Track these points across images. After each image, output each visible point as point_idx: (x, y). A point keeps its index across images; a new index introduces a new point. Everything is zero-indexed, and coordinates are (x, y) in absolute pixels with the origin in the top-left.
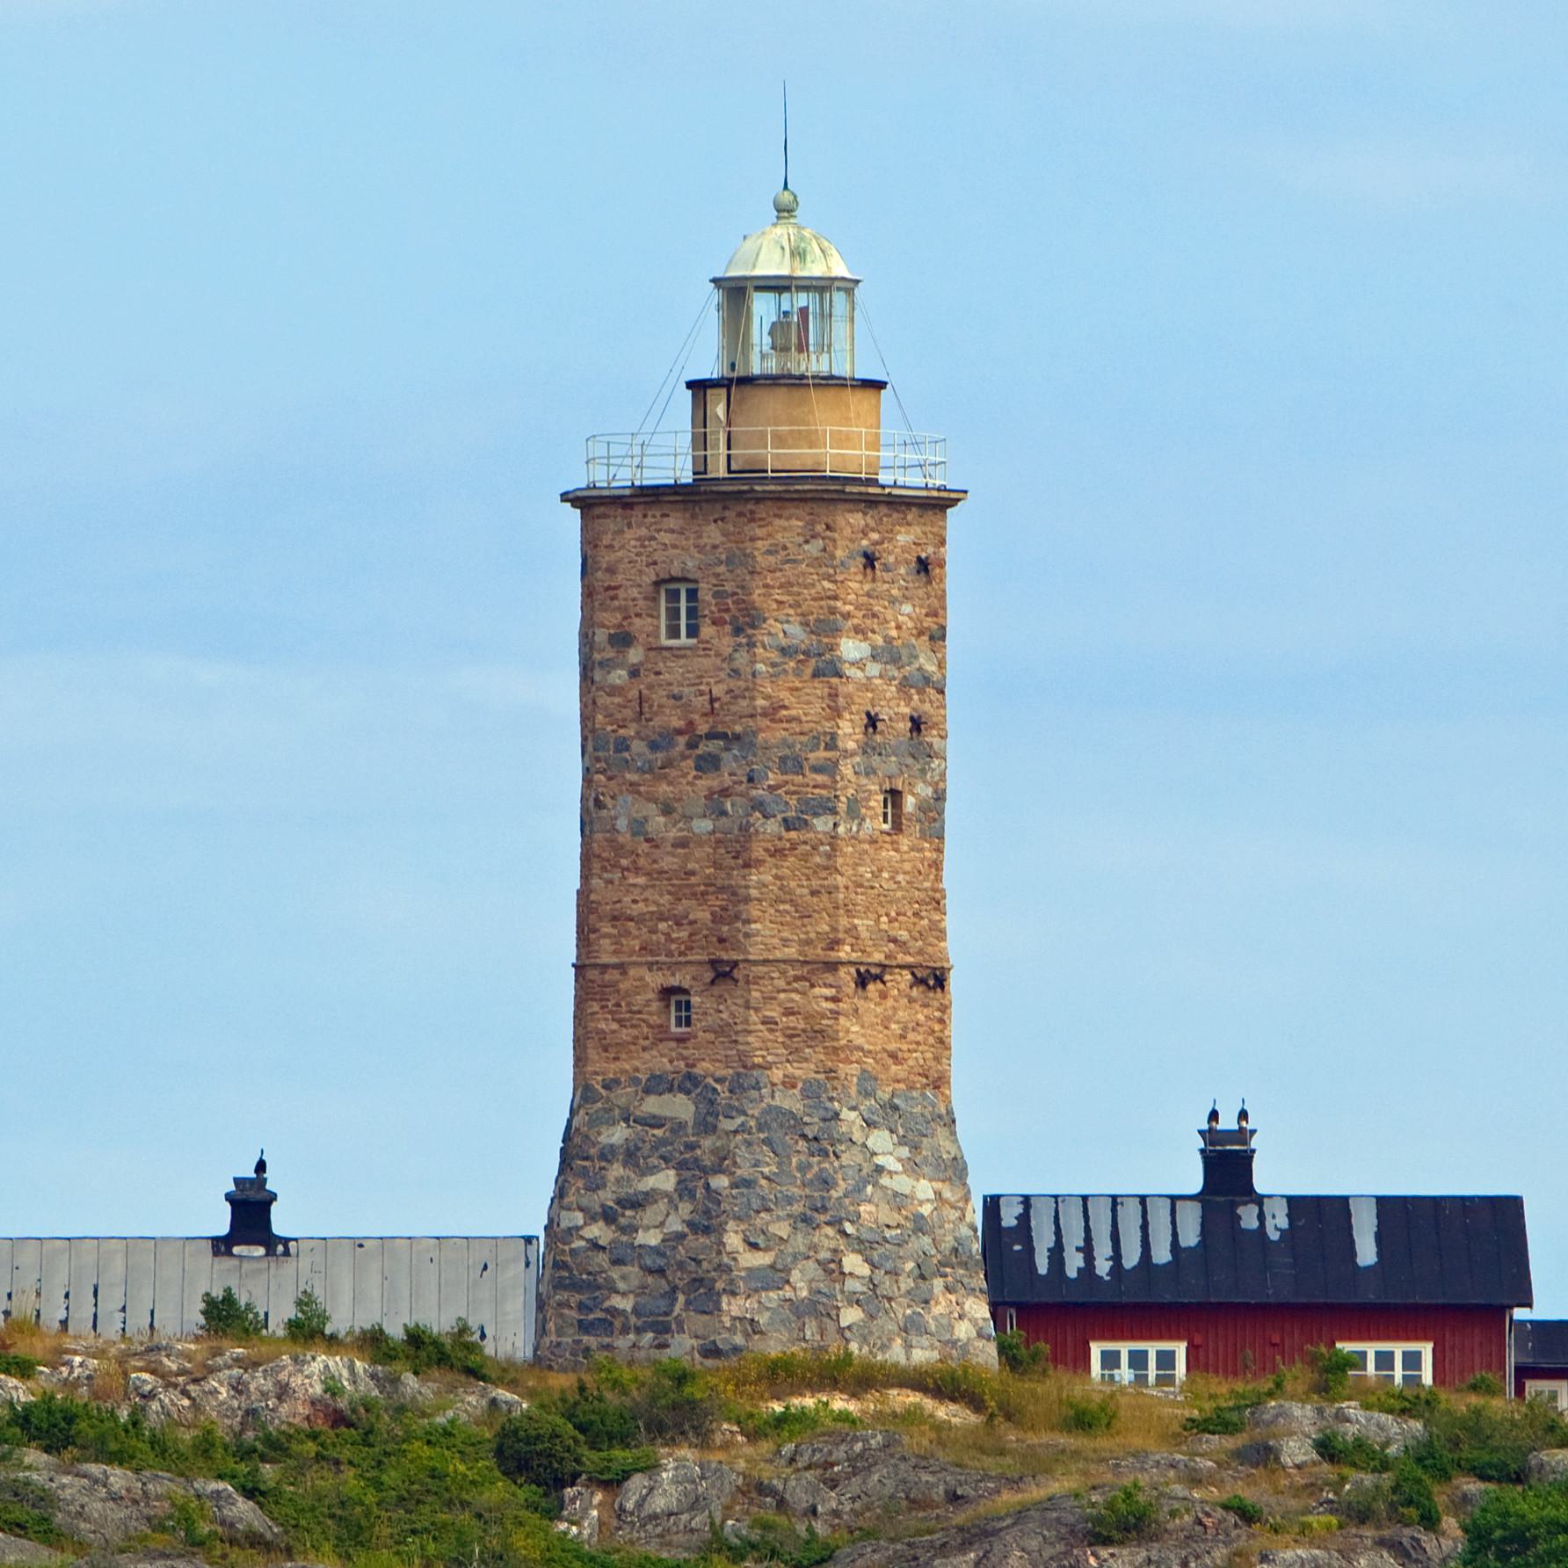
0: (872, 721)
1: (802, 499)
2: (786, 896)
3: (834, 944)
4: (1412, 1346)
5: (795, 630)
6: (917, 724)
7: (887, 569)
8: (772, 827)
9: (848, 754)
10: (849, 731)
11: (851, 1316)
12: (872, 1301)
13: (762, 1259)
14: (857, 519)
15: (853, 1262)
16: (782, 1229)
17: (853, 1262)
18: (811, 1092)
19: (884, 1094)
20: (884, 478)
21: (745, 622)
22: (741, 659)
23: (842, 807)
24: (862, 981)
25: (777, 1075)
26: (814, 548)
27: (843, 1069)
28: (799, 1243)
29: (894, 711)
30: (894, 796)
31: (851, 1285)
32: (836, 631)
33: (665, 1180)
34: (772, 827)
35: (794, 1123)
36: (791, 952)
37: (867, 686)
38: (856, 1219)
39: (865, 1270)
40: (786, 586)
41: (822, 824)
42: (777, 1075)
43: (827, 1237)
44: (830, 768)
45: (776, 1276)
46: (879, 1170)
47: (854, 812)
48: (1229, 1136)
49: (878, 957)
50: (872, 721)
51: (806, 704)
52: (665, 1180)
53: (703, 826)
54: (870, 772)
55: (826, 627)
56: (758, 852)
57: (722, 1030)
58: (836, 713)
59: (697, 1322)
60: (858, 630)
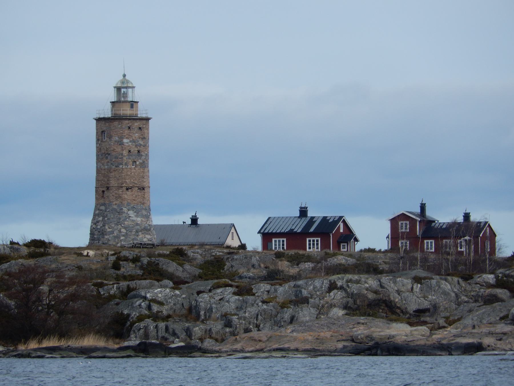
0: (130, 151)
1: (117, 119)
2: (115, 177)
3: (122, 184)
4: (283, 239)
5: (117, 138)
6: (139, 151)
7: (133, 129)
8: (114, 167)
9: (125, 156)
10: (125, 153)
11: (122, 238)
12: (126, 235)
13: (111, 230)
14: (127, 122)
15: (123, 230)
16: (113, 226)
17: (123, 230)
18: (119, 206)
19: (132, 205)
20: (139, 116)
21: (110, 137)
22: (110, 142)
23: (124, 164)
24: (127, 189)
25: (114, 203)
26: (119, 126)
27: (123, 202)
28: (116, 227)
29: (134, 150)
30: (135, 162)
31: (122, 233)
32: (123, 138)
33: (101, 219)
34: (114, 167)
35: (115, 210)
36: (116, 185)
37: (129, 146)
38: (124, 224)
39: (125, 231)
40: (116, 132)
41: (121, 166)
42: (114, 203)
43: (119, 226)
44: (122, 158)
45: (112, 232)
46: (130, 217)
47: (126, 164)
48: (304, 208)
49: (131, 185)
50: (130, 151)
51: (119, 149)
52: (101, 219)
53: (106, 167)
54: (129, 158)
55: (121, 138)
56: (112, 171)
57: (108, 197)
58: (123, 150)
59: (102, 239)
60: (127, 138)
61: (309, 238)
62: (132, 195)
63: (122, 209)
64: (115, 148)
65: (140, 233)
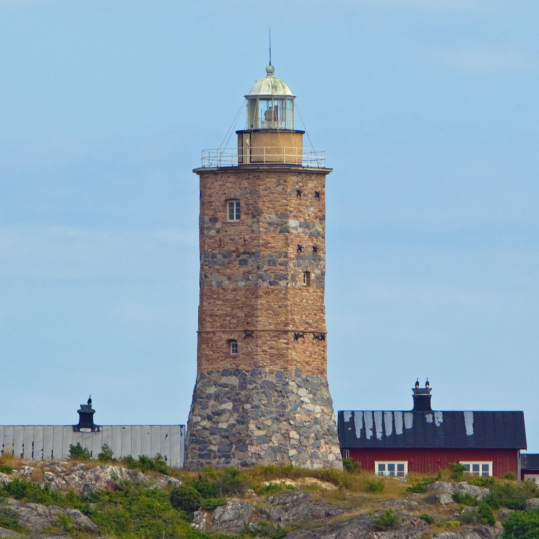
0: (300, 248)
1: (276, 172)
2: (270, 308)
3: (287, 324)
4: (485, 463)
5: (273, 217)
6: (315, 249)
7: (305, 195)
8: (266, 284)
9: (291, 259)
10: (292, 251)
11: (292, 452)
12: (300, 447)
13: (262, 433)
14: (294, 178)
15: (293, 434)
16: (269, 423)
17: (293, 434)
18: (279, 375)
19: (304, 376)
20: (304, 164)
21: (256, 214)
23: (289, 277)
24: (296, 337)
25: (267, 369)
26: (280, 188)
27: (290, 367)
28: (275, 427)
29: (307, 245)
30: (307, 274)
31: (293, 442)
32: (287, 217)
33: (229, 406)
34: (266, 284)
35: (273, 386)
36: (272, 327)
37: (298, 236)
38: (294, 419)
39: (297, 437)
40: (270, 201)
41: (282, 283)
42: (267, 369)
44: (285, 264)
45: (267, 439)
46: (302, 402)
47: (293, 279)
48: (423, 390)
49: (302, 329)
50: (300, 248)
51: (277, 242)
52: (229, 406)
53: (242, 284)
54: (299, 265)
55: (284, 216)
56: (261, 293)
57: (248, 354)
58: (287, 245)
59: (240, 454)
60: (295, 217)
61: (379, 460)
62: (304, 352)
63: (288, 383)
64: (270, 239)
65: (322, 441)
